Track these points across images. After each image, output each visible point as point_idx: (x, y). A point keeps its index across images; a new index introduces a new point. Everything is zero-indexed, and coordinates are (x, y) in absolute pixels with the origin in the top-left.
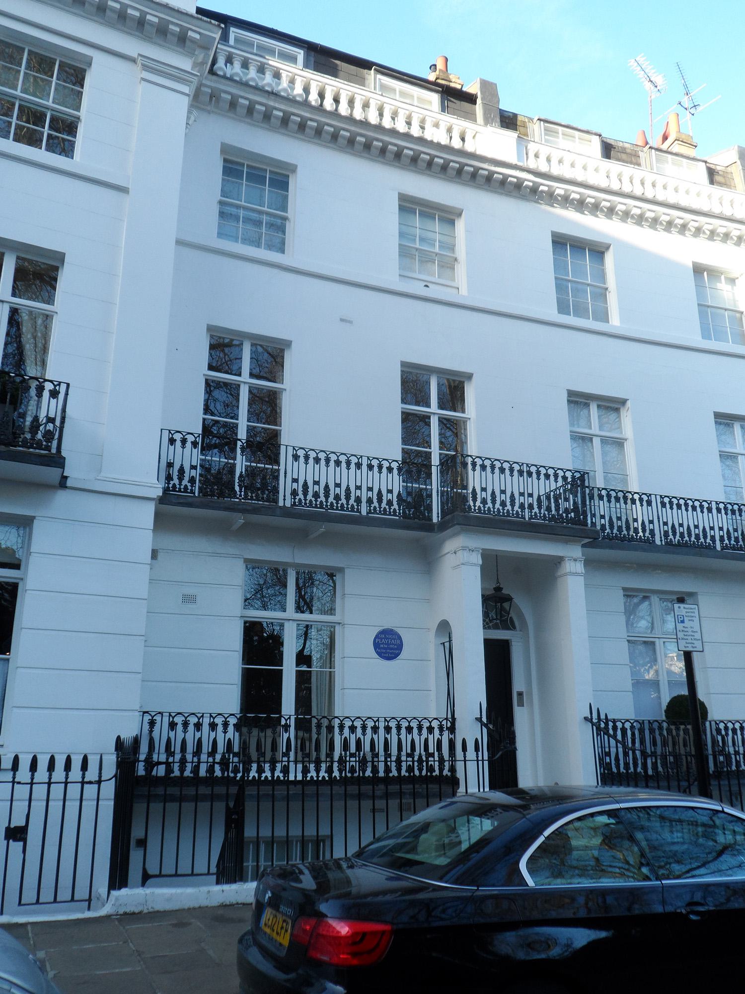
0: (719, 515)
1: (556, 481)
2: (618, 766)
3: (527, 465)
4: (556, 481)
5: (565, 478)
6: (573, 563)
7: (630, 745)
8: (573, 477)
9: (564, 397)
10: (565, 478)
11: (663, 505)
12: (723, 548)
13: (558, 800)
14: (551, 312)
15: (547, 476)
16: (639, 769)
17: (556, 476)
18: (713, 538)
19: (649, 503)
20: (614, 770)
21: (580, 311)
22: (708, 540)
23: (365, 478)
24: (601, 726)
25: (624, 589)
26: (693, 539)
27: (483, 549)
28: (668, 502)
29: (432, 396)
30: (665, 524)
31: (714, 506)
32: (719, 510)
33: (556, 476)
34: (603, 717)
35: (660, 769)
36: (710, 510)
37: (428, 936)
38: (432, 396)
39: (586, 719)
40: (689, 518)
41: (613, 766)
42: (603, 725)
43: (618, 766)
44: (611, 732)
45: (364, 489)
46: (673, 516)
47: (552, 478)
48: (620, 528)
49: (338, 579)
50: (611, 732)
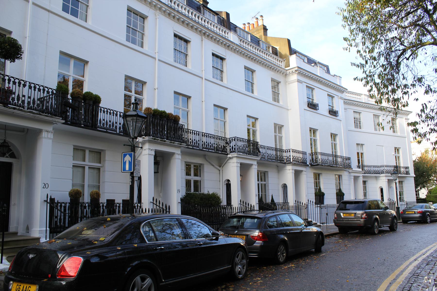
1: (44, 93)
2: (60, 222)
3: (30, 83)
4: (44, 93)
5: (48, 92)
7: (85, 215)
9: (283, 125)
10: (48, 92)
12: (120, 132)
13: (152, 237)
14: (123, 39)
15: (39, 90)
16: (62, 224)
17: (44, 90)
18: (116, 127)
20: (58, 224)
21: (134, 42)
22: (114, 128)
23: (204, 139)
24: (52, 204)
25: (74, 146)
26: (108, 126)
27: (155, 150)
29: (134, 85)
30: (203, 142)
32: (30, 87)
33: (44, 90)
36: (116, 115)
37: (129, 269)
38: (134, 85)
39: (45, 201)
41: (58, 222)
43: (60, 222)
44: (59, 208)
45: (27, 97)
46: (204, 139)
48: (103, 124)
49: (102, 153)
50: (59, 208)
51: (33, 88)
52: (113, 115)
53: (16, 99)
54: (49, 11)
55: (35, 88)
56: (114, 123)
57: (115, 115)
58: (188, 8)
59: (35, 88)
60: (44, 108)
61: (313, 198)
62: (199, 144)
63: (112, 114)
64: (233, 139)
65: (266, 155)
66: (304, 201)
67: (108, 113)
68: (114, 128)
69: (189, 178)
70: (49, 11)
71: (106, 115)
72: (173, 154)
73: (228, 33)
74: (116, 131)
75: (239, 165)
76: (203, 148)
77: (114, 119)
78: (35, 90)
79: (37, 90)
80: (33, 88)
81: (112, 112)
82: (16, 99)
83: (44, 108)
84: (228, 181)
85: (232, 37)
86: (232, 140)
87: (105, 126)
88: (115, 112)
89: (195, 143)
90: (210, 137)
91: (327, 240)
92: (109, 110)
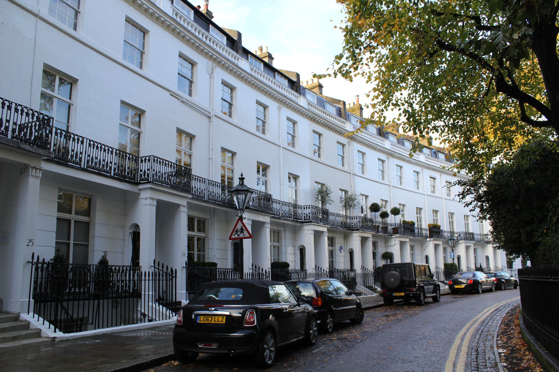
0: (16, 114)
3: (16, 104)
6: (145, 200)
8: (43, 118)
11: (90, 145)
12: (114, 174)
16: (42, 291)
17: (33, 115)
18: (111, 168)
19: (82, 142)
23: (94, 153)
28: (93, 144)
30: (89, 156)
31: (13, 106)
32: (16, 110)
33: (33, 115)
34: (41, 260)
35: (49, 291)
36: (9, 108)
40: (101, 155)
42: (40, 265)
46: (94, 153)
47: (30, 116)
48: (96, 163)
51: (20, 112)
52: (93, 148)
53: (17, 131)
54: (36, 15)
55: (22, 111)
56: (109, 163)
57: (80, 142)
58: (196, 25)
59: (22, 111)
60: (32, 138)
61: (505, 264)
62: (81, 159)
63: (107, 151)
64: (147, 158)
65: (151, 173)
66: (500, 266)
67: (103, 150)
68: (78, 160)
69: (201, 235)
70: (36, 15)
71: (92, 149)
72: (178, 206)
73: (238, 59)
74: (110, 173)
75: (155, 203)
76: (87, 167)
77: (109, 157)
78: (22, 114)
79: (24, 114)
80: (20, 112)
81: (107, 148)
82: (17, 131)
83: (32, 138)
84: (137, 226)
85: (244, 64)
86: (145, 160)
87: (98, 166)
88: (111, 149)
89: (103, 165)
90: (97, 147)
91: (171, 351)
92: (103, 146)
